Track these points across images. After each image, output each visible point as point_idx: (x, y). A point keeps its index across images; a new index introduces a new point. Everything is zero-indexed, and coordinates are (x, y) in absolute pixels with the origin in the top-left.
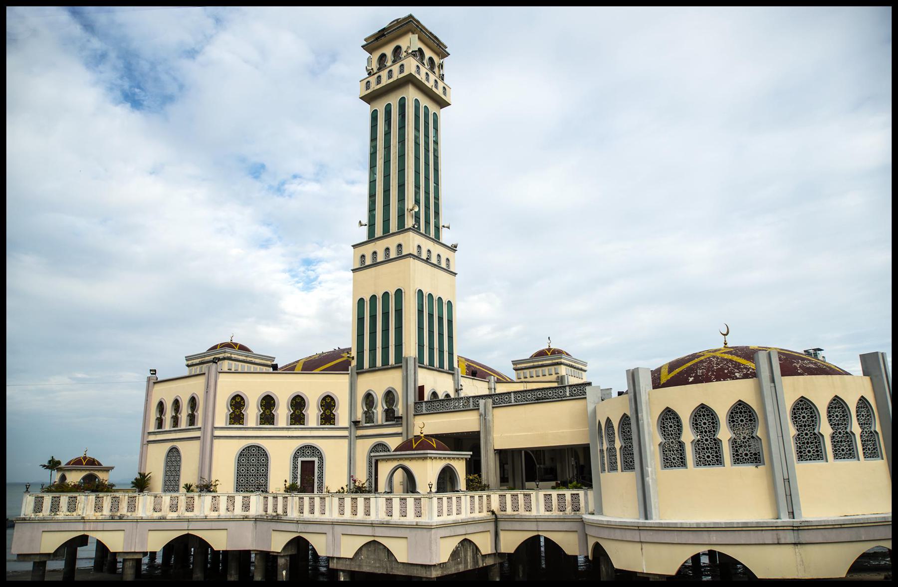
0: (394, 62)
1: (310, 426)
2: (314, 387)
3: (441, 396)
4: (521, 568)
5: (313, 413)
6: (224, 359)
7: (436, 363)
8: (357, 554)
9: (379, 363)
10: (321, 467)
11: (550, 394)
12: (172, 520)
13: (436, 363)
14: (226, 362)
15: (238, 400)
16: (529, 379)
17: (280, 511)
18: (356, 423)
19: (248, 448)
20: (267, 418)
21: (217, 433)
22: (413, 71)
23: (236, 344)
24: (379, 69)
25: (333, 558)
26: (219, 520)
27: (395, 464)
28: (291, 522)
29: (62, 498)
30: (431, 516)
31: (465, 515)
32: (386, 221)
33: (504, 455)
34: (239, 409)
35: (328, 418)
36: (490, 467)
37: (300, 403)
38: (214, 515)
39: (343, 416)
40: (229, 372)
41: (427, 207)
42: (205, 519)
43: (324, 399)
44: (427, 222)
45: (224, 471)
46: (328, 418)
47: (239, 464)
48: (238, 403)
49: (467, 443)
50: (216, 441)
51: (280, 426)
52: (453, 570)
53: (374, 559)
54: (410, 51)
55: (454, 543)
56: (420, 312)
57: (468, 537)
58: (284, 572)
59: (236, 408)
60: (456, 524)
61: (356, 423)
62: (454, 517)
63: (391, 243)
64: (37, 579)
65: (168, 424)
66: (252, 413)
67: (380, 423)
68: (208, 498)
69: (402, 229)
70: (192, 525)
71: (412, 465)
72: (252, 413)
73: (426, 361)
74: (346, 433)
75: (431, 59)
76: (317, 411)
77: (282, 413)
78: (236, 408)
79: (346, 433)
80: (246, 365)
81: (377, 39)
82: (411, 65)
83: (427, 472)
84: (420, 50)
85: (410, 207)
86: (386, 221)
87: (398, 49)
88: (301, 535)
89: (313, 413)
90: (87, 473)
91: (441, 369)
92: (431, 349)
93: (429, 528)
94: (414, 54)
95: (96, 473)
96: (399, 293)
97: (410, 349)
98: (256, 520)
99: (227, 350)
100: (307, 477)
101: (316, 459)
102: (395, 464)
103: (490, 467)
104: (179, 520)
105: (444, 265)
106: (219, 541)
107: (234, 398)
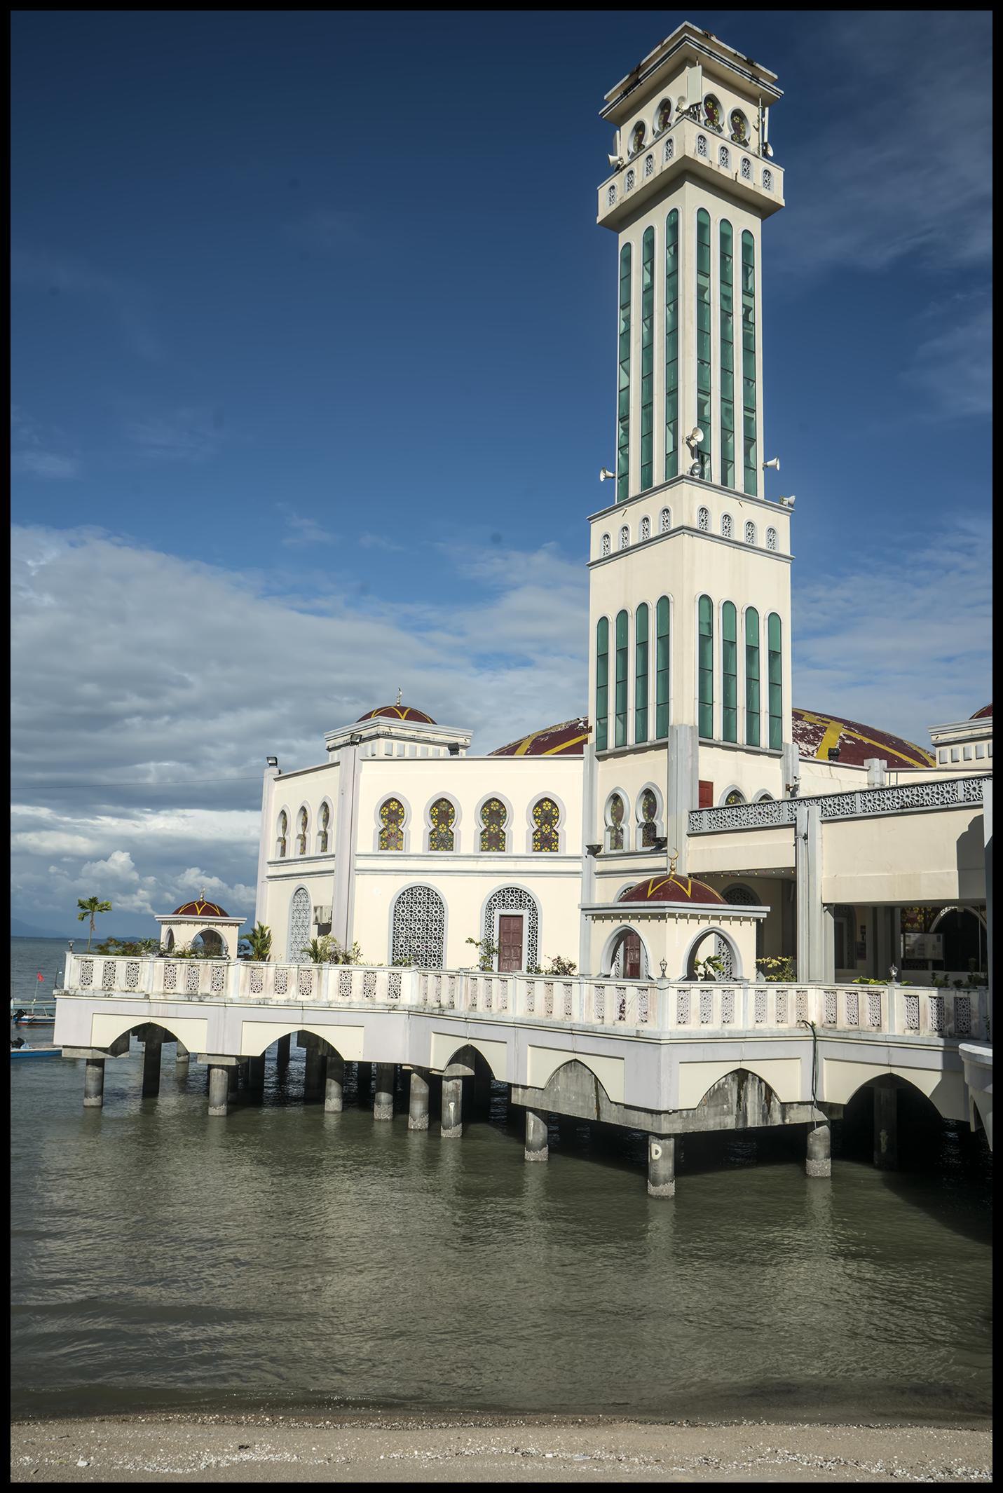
0: (658, 135)
1: (515, 852)
2: (523, 782)
3: (750, 796)
4: (883, 1133)
5: (519, 829)
6: (377, 736)
7: (741, 736)
8: (552, 1081)
9: (631, 740)
10: (534, 928)
11: (927, 796)
12: (278, 1007)
13: (741, 736)
14: (382, 742)
15: (394, 806)
16: (950, 765)
17: (866, 1020)
18: (594, 850)
19: (411, 890)
20: (442, 840)
21: (360, 864)
22: (690, 149)
23: (402, 709)
24: (633, 157)
25: (517, 1086)
26: (349, 1009)
27: (704, 925)
28: (457, 1019)
29: (403, 975)
30: (666, 1023)
31: (742, 1022)
32: (647, 467)
33: (844, 915)
34: (396, 822)
35: (546, 840)
36: (816, 938)
37: (498, 812)
38: (342, 1001)
39: (572, 834)
40: (389, 758)
41: (727, 431)
42: (329, 1007)
43: (539, 804)
44: (727, 462)
45: (371, 932)
46: (546, 840)
47: (397, 918)
48: (392, 812)
49: (773, 894)
50: (360, 880)
51: (463, 852)
52: (712, 1122)
53: (575, 1093)
54: (685, 107)
55: (714, 1074)
56: (705, 640)
57: (477, 1045)
58: (452, 1105)
59: (391, 821)
60: (715, 1040)
61: (594, 850)
62: (714, 1027)
63: (652, 506)
64: (741, 1126)
65: (313, 848)
66: (417, 827)
67: (632, 849)
68: (332, 973)
69: (673, 477)
70: (310, 1017)
71: (641, 928)
72: (417, 827)
73: (718, 732)
74: (577, 866)
75: (738, 114)
76: (375, 826)
77: (468, 828)
78: (391, 821)
79: (577, 866)
80: (419, 745)
81: (626, 93)
82: (688, 138)
83: (669, 940)
84: (711, 100)
85: (689, 434)
86: (647, 467)
87: (665, 105)
88: (895, 1071)
89: (519, 829)
90: (205, 927)
91: (752, 746)
92: (729, 708)
93: (656, 1042)
94: (692, 113)
95: (218, 929)
96: (664, 602)
97: (684, 711)
98: (411, 1012)
99: (382, 719)
100: (509, 940)
101: (525, 913)
102: (704, 925)
103: (816, 938)
104: (288, 1006)
105: (762, 542)
106: (352, 1047)
107: (488, 803)
